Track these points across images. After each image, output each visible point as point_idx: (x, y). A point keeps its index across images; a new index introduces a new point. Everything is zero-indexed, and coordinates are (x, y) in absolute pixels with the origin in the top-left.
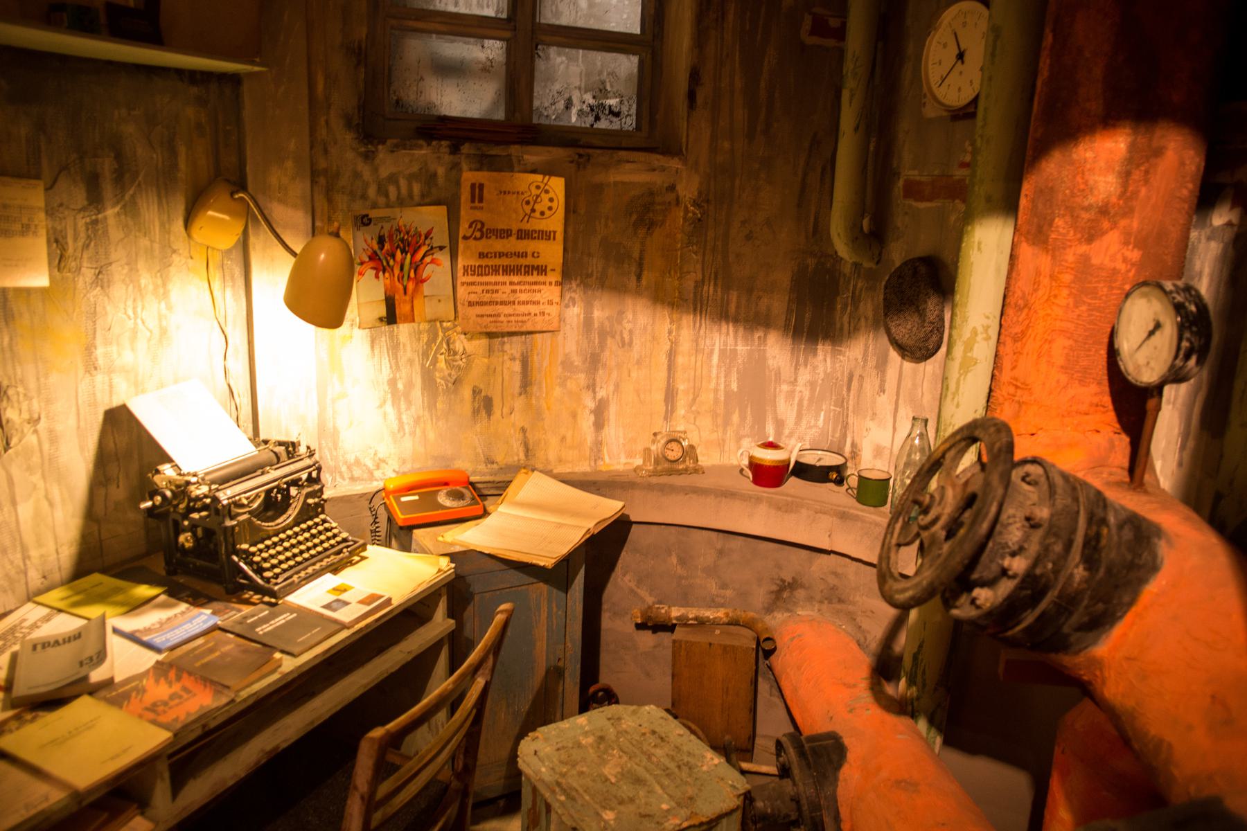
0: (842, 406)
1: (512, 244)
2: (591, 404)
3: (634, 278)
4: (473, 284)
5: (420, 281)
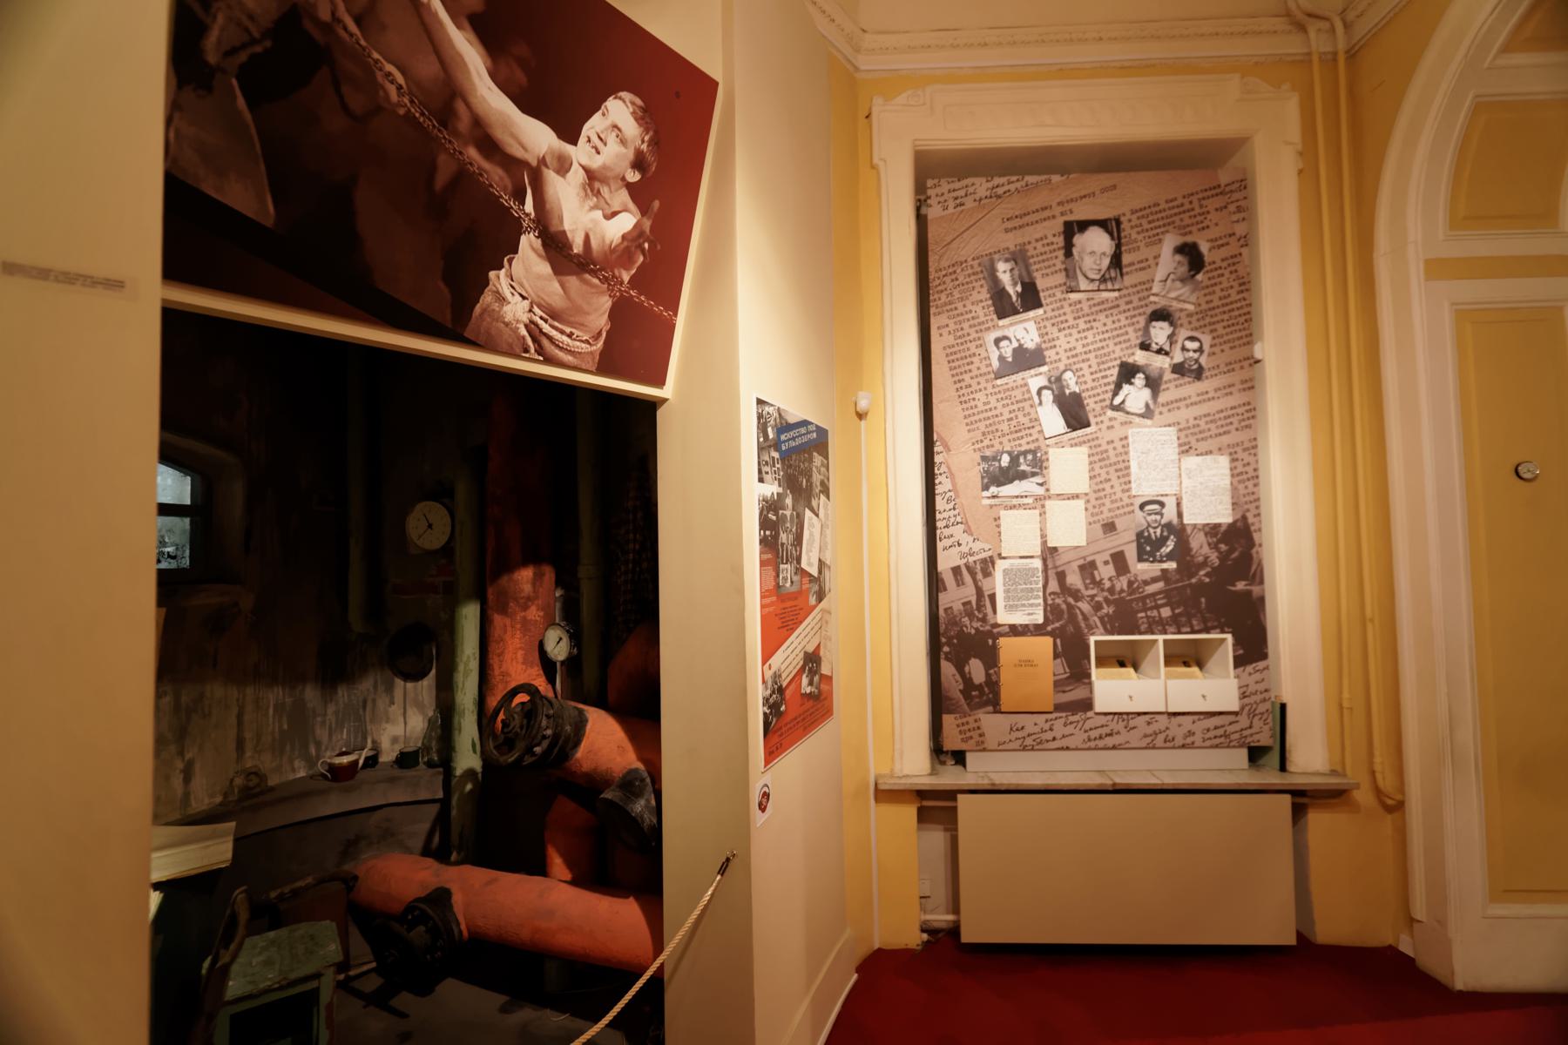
2: (180, 765)
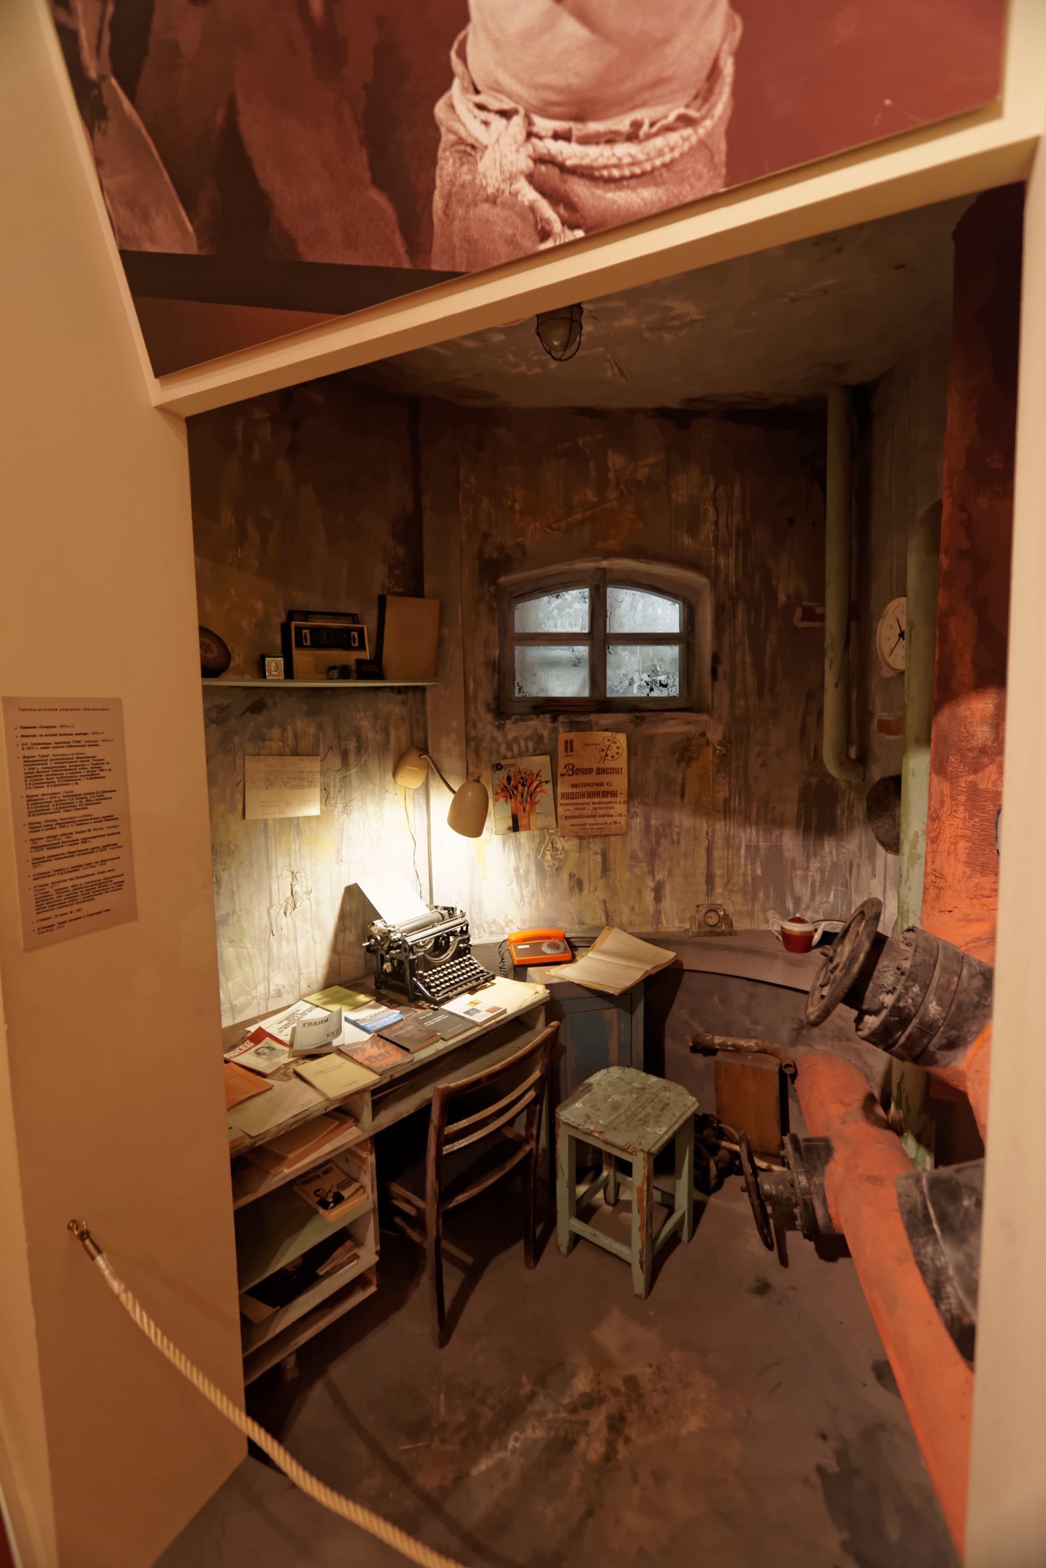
0: (846, 887)
1: (593, 778)
3: (678, 797)
4: (568, 804)
5: (533, 804)
